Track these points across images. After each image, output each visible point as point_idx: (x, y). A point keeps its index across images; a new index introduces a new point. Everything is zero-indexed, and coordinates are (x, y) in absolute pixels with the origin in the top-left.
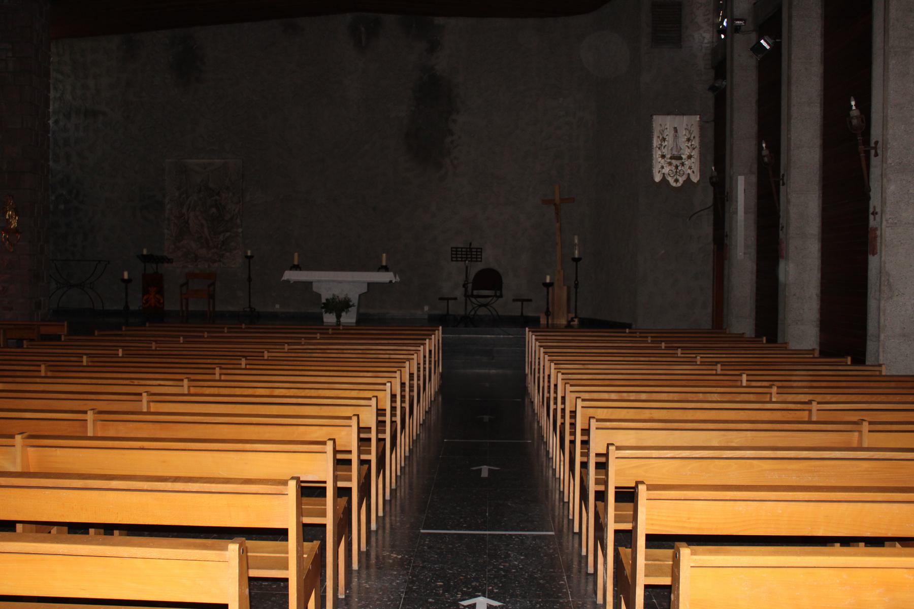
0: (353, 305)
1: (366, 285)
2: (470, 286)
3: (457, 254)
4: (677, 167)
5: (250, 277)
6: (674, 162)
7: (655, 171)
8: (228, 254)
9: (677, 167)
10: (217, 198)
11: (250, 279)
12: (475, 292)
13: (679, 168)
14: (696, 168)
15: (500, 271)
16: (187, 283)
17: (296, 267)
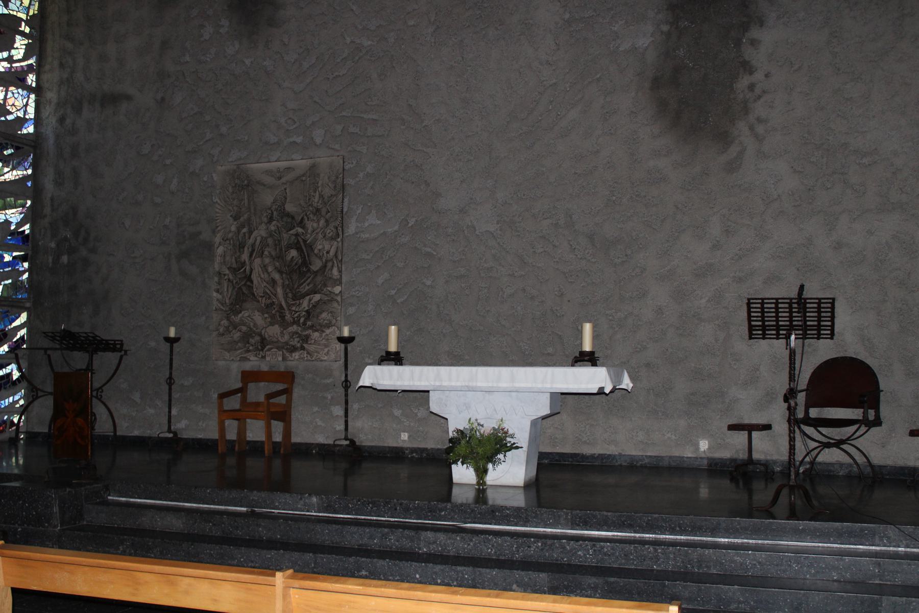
0: (514, 447)
1: (545, 401)
2: (801, 398)
3: (769, 319)
5: (170, 378)
8: (316, 334)
10: (300, 230)
11: (170, 381)
12: (814, 413)
15: (869, 361)
16: (242, 390)
17: (395, 359)
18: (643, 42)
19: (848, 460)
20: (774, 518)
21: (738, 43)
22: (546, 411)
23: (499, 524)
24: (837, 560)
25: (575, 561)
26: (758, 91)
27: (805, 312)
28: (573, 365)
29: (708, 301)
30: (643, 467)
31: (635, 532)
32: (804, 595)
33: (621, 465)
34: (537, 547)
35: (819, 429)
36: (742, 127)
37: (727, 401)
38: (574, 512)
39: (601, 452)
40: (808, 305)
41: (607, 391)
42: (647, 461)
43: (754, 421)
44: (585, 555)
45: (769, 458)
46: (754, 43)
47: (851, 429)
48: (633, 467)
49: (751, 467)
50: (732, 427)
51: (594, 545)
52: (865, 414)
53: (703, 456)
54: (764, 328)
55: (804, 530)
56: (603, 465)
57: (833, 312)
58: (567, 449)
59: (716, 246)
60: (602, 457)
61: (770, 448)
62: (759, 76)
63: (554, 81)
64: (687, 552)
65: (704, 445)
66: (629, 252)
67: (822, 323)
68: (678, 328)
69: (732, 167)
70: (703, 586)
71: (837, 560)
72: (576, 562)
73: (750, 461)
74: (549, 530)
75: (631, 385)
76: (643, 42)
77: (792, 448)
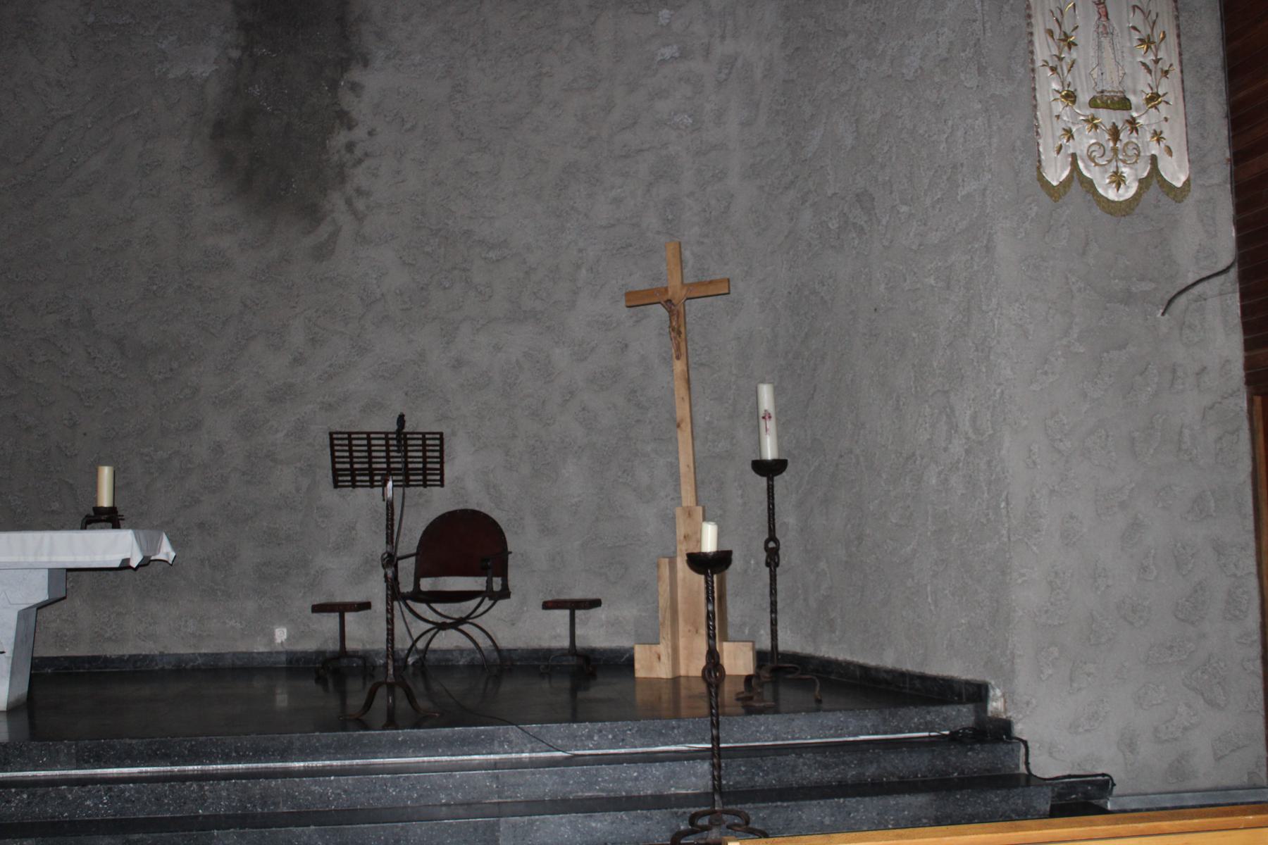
2: (407, 568)
3: (353, 462)
4: (1115, 134)
6: (1106, 117)
7: (1047, 148)
9: (1115, 134)
12: (426, 584)
13: (1123, 136)
14: (1175, 135)
15: (496, 515)
18: (203, 70)
19: (468, 644)
20: (367, 728)
21: (334, 85)
22: (42, 596)
23: (118, 766)
24: (445, 777)
25: (80, 816)
26: (358, 152)
27: (406, 451)
28: (84, 528)
29: (287, 435)
30: (196, 670)
31: (173, 764)
32: (402, 828)
33: (163, 669)
34: (21, 801)
35: (434, 605)
36: (336, 200)
37: (313, 572)
38: (81, 743)
39: (134, 652)
40: (410, 442)
41: (134, 564)
42: (200, 661)
43: (349, 599)
44: (98, 806)
45: (368, 647)
46: (355, 87)
47: (473, 603)
48: (183, 670)
49: (345, 662)
50: (318, 609)
51: (110, 789)
52: (489, 583)
53: (280, 649)
54: (353, 472)
55: (404, 742)
56: (137, 670)
57: (442, 451)
58: (83, 650)
59: (298, 360)
60: (134, 659)
61: (364, 634)
62: (359, 133)
63: (69, 112)
64: (245, 785)
65: (281, 634)
66: (175, 365)
67: (429, 466)
68: (244, 474)
69: (322, 252)
70: (266, 832)
71: (445, 777)
72: (84, 817)
73: (343, 653)
74: (42, 773)
75: (173, 554)
76: (203, 70)
77: (391, 632)
